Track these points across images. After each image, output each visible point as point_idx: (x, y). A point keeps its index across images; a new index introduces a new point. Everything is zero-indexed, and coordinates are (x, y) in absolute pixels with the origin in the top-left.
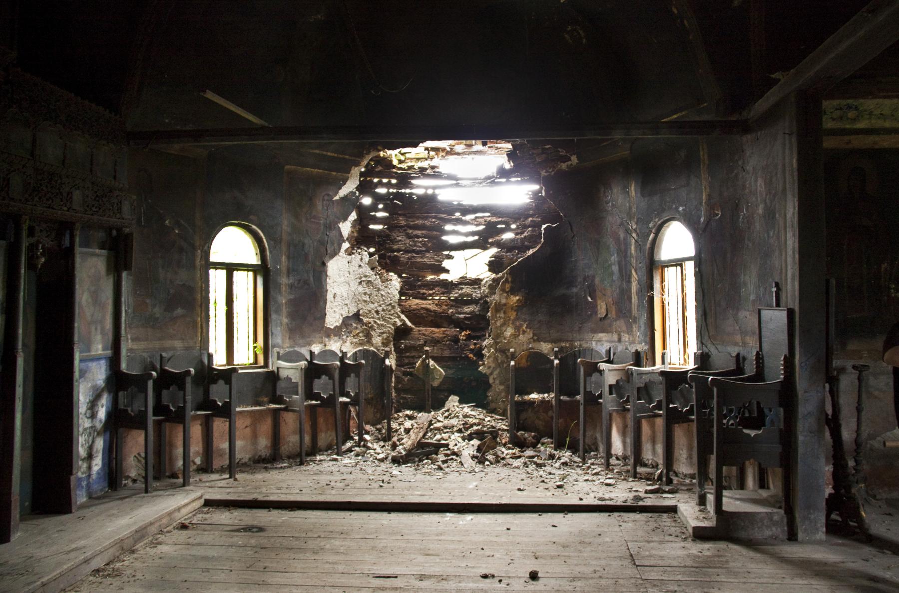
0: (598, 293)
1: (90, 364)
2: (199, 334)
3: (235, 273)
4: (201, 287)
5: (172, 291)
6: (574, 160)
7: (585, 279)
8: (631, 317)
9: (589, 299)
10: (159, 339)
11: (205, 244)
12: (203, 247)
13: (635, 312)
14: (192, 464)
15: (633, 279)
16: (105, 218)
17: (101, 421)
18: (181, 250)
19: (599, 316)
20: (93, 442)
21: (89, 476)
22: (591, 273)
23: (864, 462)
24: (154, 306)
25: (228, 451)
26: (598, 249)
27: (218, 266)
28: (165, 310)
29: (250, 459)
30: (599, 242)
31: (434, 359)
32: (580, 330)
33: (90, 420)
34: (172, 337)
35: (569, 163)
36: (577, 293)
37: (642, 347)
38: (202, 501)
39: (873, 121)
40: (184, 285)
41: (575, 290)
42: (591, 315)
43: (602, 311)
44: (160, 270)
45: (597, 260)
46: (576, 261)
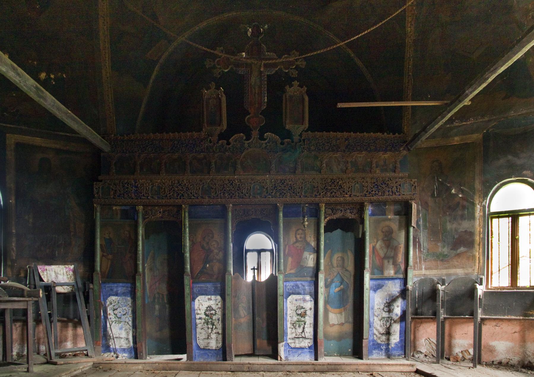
1: (387, 282)
2: (477, 265)
3: (521, 218)
4: (480, 231)
5: (456, 237)
10: (446, 268)
11: (483, 200)
12: (482, 203)
16: (385, 197)
17: (397, 315)
18: (464, 207)
20: (390, 325)
21: (388, 344)
23: (493, 343)
24: (444, 247)
27: (499, 215)
28: (451, 249)
29: (519, 362)
33: (387, 313)
34: (455, 267)
38: (414, 369)
40: (466, 231)
44: (448, 224)
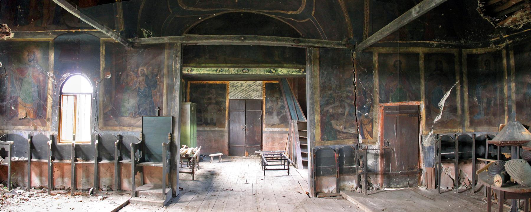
0: (20, 105)
6: (12, 35)
7: (11, 98)
8: (45, 118)
9: (13, 108)
13: (49, 115)
14: (56, 39)
15: (48, 100)
19: (19, 117)
22: (16, 95)
25: (264, 126)
26: (21, 83)
30: (22, 80)
31: (300, 36)
32: (7, 124)
35: (8, 36)
36: (6, 105)
37: (56, 133)
39: (51, 79)
41: (5, 103)
42: (13, 117)
43: (22, 113)
45: (21, 89)
46: (7, 88)
